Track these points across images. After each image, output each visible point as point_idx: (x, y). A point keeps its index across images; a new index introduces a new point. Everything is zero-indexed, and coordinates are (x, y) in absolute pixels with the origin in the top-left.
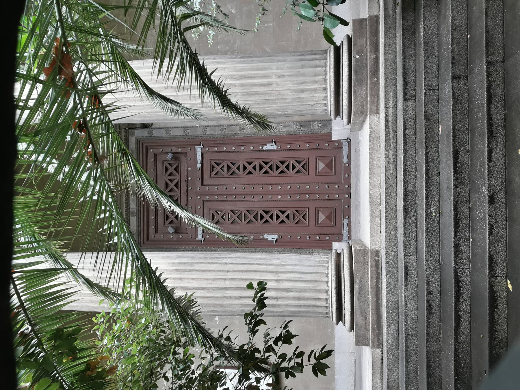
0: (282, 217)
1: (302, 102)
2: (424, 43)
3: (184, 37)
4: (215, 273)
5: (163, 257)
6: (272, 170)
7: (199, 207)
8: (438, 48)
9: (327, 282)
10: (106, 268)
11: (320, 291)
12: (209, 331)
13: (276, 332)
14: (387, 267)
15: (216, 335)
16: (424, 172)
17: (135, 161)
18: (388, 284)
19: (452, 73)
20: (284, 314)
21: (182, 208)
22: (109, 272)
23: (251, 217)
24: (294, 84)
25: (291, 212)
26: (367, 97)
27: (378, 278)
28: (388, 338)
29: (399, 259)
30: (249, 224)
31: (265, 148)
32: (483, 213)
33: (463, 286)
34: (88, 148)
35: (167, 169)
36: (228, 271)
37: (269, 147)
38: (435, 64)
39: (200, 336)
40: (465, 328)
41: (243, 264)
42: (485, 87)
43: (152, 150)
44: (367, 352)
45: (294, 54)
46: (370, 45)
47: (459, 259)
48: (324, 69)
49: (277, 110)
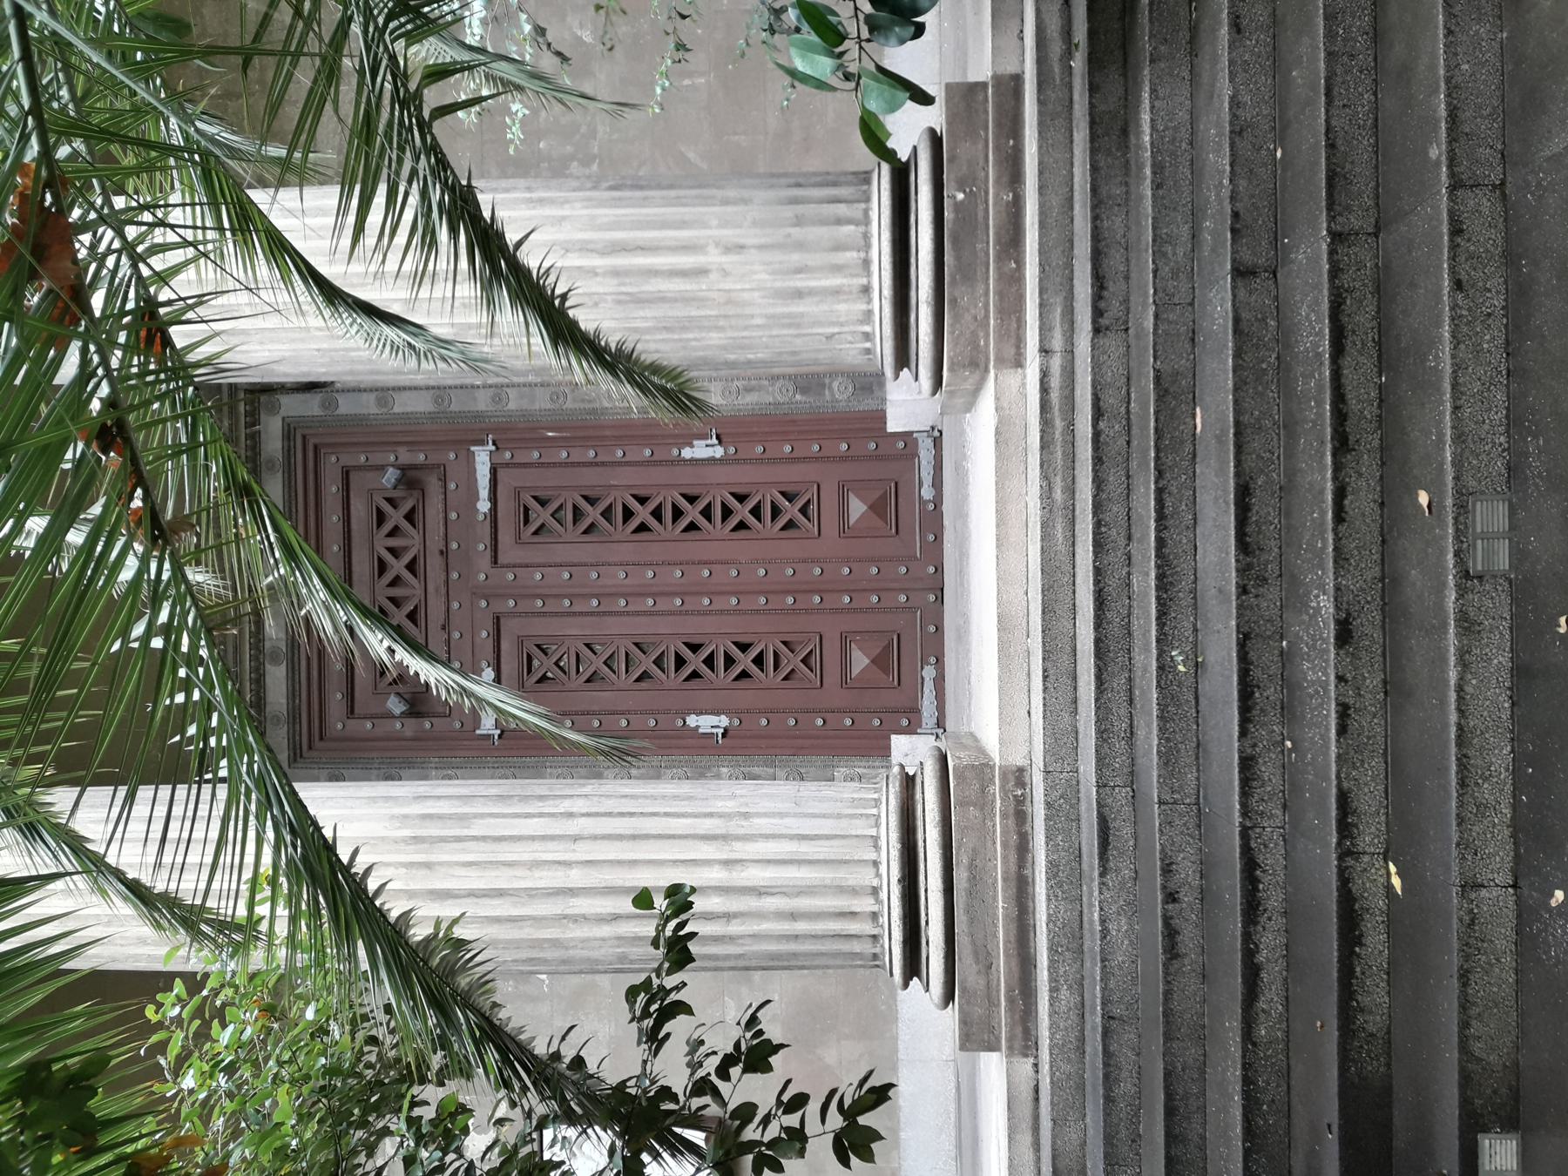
0: (742, 662)
1: (798, 326)
2: (1153, 166)
3: (434, 138)
4: (537, 845)
5: (373, 799)
6: (709, 520)
7: (484, 634)
8: (1192, 184)
9: (876, 864)
10: (193, 858)
11: (854, 891)
12: (522, 1037)
13: (722, 1041)
14: (1048, 818)
15: (540, 1049)
16: (1153, 544)
17: (278, 517)
18: (1053, 867)
19: (1234, 261)
20: (746, 963)
21: (431, 657)
22: (205, 876)
23: (646, 663)
24: (773, 273)
25: (770, 646)
26: (987, 316)
27: (1023, 848)
28: (1053, 1027)
29: (1081, 795)
30: (643, 685)
31: (687, 453)
32: (1320, 670)
33: (1266, 879)
34: (131, 498)
35: (381, 518)
36: (576, 838)
37: (701, 450)
38: (1185, 230)
39: (492, 1056)
40: (1271, 999)
41: (622, 814)
42: (1325, 306)
43: (333, 459)
44: (993, 1068)
45: (775, 181)
46: (998, 162)
47: (1253, 801)
48: (862, 229)
49: (724, 348)
